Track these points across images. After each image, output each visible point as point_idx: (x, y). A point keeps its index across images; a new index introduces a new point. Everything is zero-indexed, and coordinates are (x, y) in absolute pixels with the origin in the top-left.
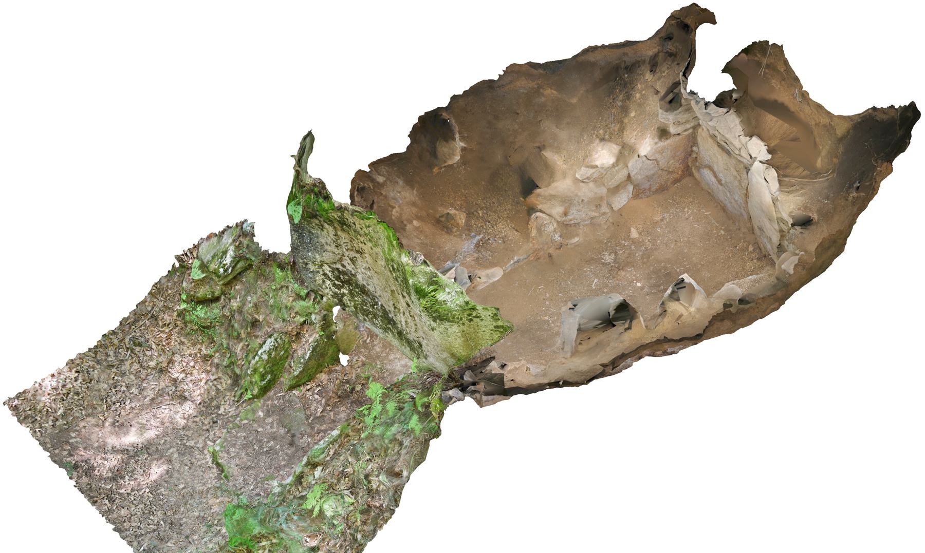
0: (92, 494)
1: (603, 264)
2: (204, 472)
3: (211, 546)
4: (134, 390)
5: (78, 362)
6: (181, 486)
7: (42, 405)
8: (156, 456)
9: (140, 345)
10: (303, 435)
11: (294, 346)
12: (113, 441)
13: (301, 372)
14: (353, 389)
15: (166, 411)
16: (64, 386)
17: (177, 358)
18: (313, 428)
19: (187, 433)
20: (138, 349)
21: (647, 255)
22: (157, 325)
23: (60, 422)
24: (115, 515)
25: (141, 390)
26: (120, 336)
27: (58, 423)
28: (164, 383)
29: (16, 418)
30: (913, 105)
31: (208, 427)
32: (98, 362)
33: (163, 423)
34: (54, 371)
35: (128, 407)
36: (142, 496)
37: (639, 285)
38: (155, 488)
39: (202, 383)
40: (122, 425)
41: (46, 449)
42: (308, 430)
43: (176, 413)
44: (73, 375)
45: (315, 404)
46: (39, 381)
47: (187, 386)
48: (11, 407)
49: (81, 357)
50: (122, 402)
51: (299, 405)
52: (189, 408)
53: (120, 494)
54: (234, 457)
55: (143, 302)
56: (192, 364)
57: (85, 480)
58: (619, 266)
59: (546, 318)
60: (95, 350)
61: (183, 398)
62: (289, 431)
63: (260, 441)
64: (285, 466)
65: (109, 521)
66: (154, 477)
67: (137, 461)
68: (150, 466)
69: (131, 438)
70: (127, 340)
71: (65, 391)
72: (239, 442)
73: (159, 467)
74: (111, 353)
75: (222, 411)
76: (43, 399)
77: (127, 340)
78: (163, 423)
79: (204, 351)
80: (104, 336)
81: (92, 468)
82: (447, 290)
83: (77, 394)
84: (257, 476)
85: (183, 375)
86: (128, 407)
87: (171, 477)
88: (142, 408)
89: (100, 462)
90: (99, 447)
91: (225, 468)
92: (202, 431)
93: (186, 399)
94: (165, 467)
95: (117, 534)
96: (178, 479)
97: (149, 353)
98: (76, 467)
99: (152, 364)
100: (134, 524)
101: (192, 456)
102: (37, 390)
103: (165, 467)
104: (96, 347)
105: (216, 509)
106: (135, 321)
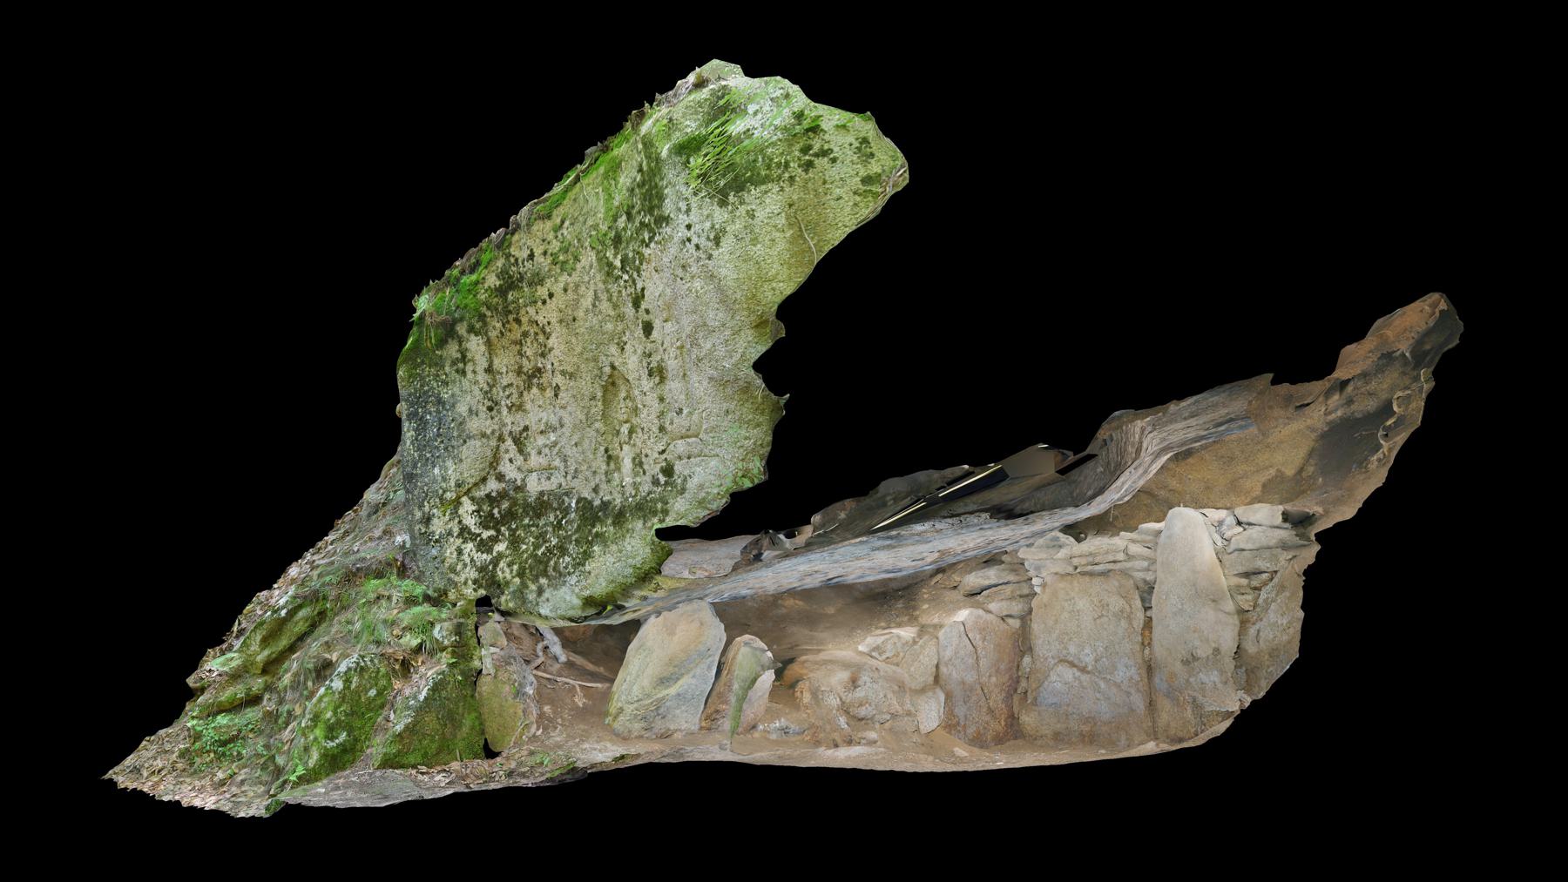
11: (397, 685)
13: (407, 727)
82: (751, 108)
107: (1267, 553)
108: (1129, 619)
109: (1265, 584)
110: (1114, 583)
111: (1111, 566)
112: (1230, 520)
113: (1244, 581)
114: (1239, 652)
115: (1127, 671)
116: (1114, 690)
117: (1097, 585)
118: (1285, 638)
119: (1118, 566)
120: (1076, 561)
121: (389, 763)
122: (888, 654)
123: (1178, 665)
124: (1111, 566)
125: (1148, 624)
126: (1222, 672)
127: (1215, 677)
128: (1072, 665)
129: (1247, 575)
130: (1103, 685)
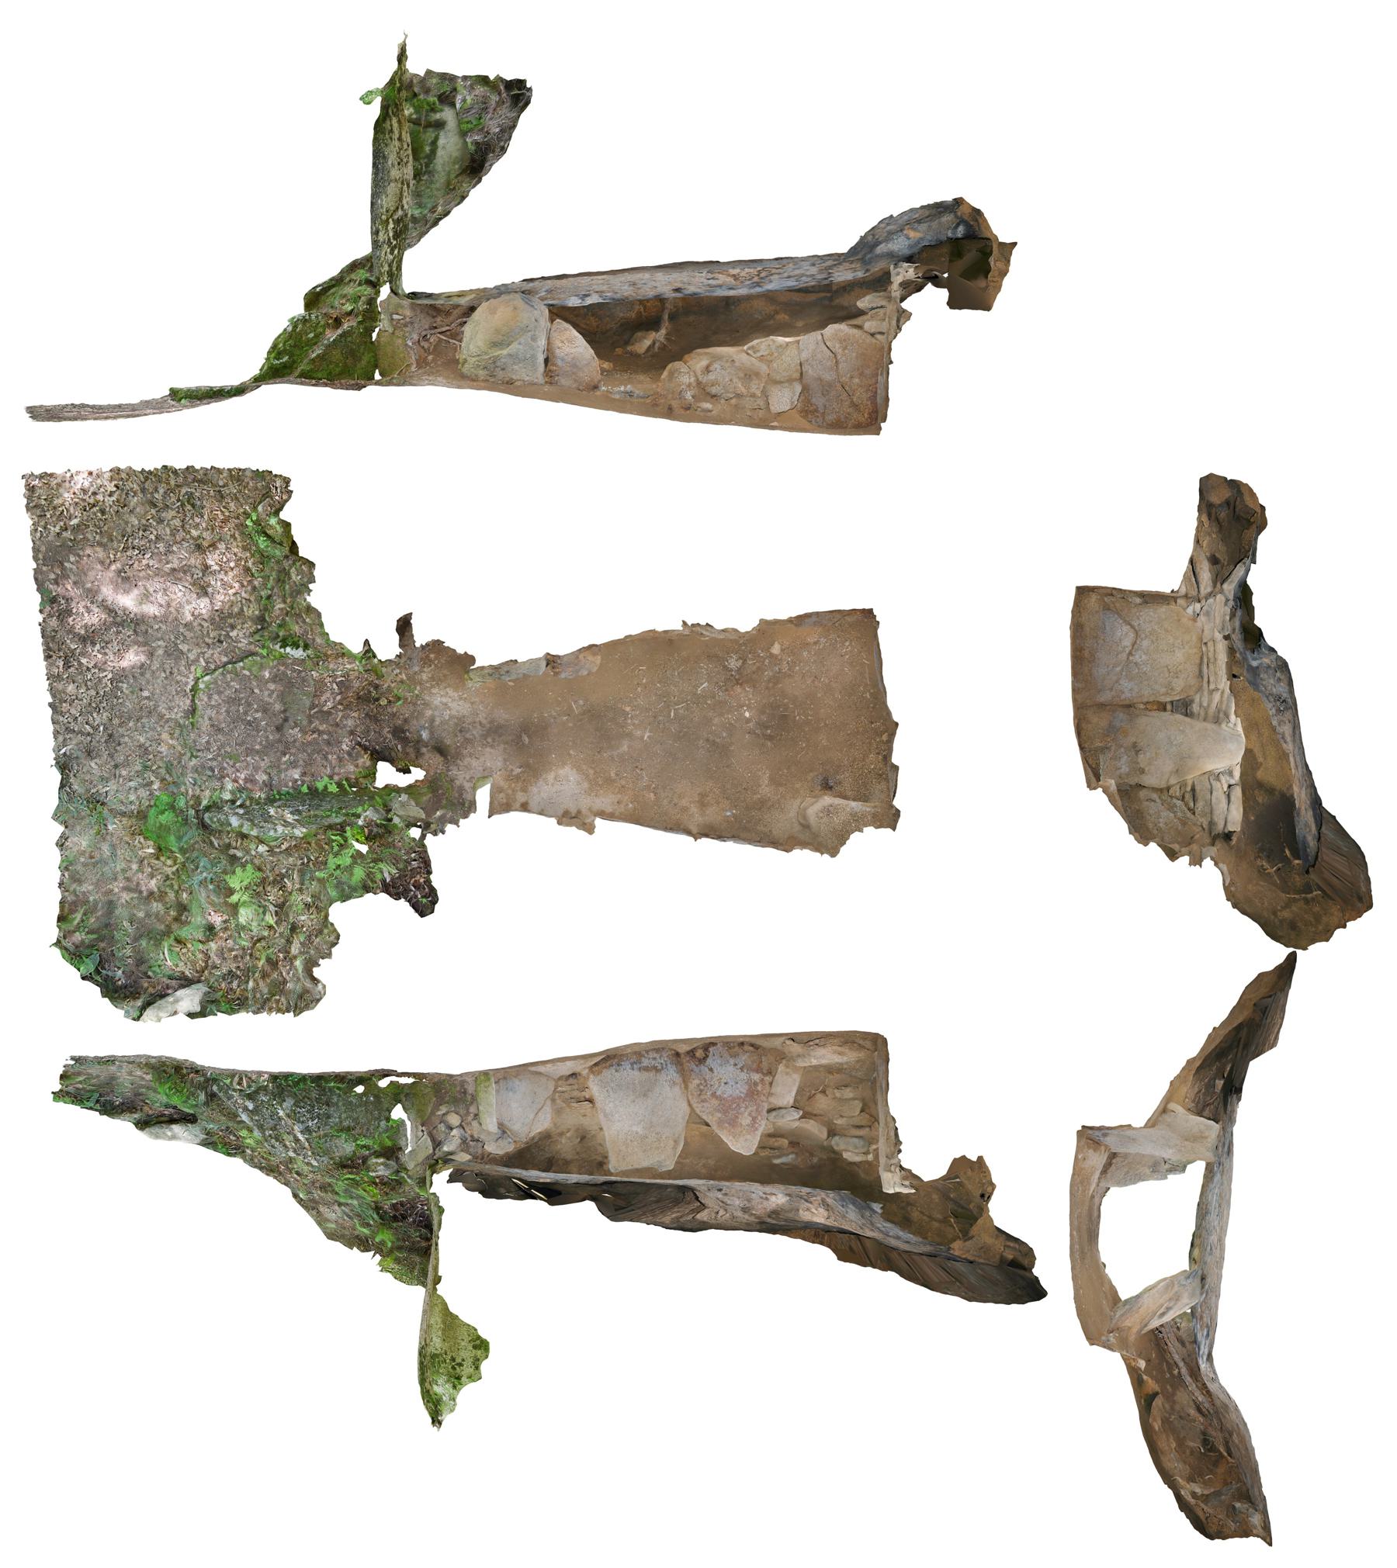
0: (53, 645)
1: (725, 667)
2: (178, 693)
3: (132, 797)
4: (161, 546)
5: (124, 476)
6: (146, 694)
7: (60, 501)
8: (140, 639)
9: (193, 506)
10: (296, 725)
12: (107, 592)
14: (377, 700)
15: (180, 594)
16: (95, 494)
17: (222, 546)
18: (311, 722)
19: (187, 633)
20: (189, 507)
21: (776, 680)
22: (220, 501)
23: (67, 535)
24: (60, 686)
25: (169, 552)
26: (181, 480)
27: (65, 534)
28: (195, 561)
29: (25, 501)
30: (1209, 484)
31: (210, 641)
32: (143, 490)
33: (169, 605)
34: (93, 469)
35: (144, 562)
36: (100, 680)
37: (747, 714)
38: (120, 676)
39: (231, 592)
40: (127, 579)
41: (35, 558)
42: (305, 723)
43: (189, 602)
44: (111, 488)
45: (328, 695)
46: (73, 471)
47: (215, 583)
48: (27, 485)
49: (130, 472)
50: (142, 551)
51: (311, 689)
52: (203, 606)
53: (80, 664)
54: (213, 707)
55: (219, 471)
56: (232, 564)
57: (54, 622)
58: (739, 679)
59: (628, 709)
60: (147, 475)
61: (203, 591)
62: (285, 711)
63: (249, 705)
64: (258, 752)
65: (51, 689)
66: (125, 664)
67: (119, 632)
68: (128, 647)
69: (127, 601)
70: (184, 491)
71: (92, 501)
72: (227, 693)
73: (137, 654)
74: (161, 491)
75: (233, 634)
76: (66, 495)
77: (184, 491)
78: (169, 605)
79: (250, 564)
80: (165, 467)
81: (69, 612)
83: (103, 512)
84: (223, 746)
85: (217, 568)
86: (144, 562)
87: (142, 674)
88: (158, 573)
89: (81, 610)
90: (90, 590)
91: (198, 713)
92: (200, 641)
93: (206, 594)
94: (143, 658)
95: (50, 711)
96: (148, 682)
97: (197, 520)
98: (53, 600)
99: (195, 533)
100: (73, 711)
101: (176, 663)
102: (65, 481)
103: (143, 658)
104: (150, 472)
105: (163, 749)
106: (200, 481)
107: (1207, 810)
108: (1167, 694)
109: (1186, 805)
110: (1193, 681)
112: (1232, 782)
113: (1189, 788)
114: (1140, 786)
115: (1128, 689)
117: (1192, 669)
118: (1151, 826)
119: (1205, 685)
120: (1210, 644)
123: (1133, 739)
125: (1162, 707)
126: (1128, 775)
127: (1125, 769)
129: (1193, 790)
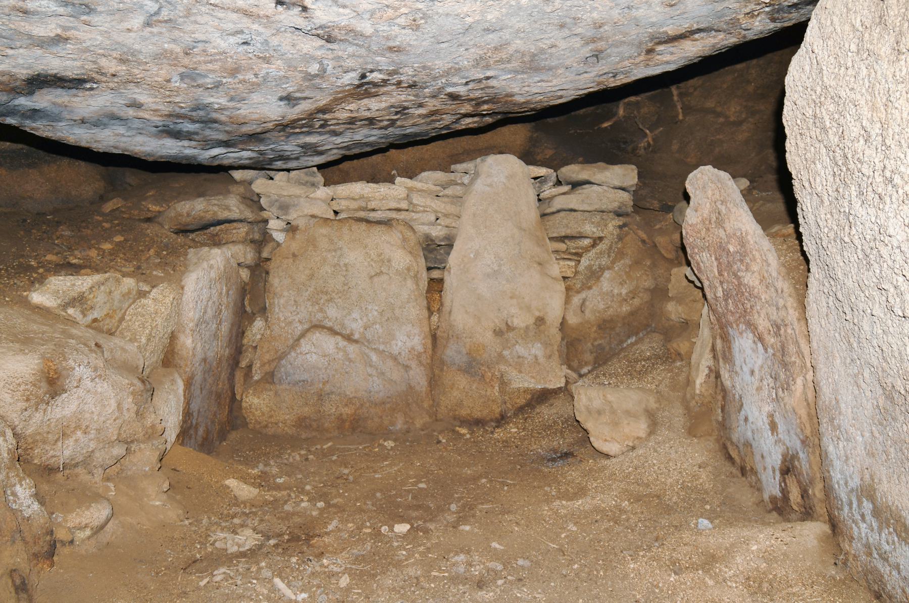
109: (587, 249)
111: (394, 215)
114: (563, 324)
116: (390, 363)
118: (626, 309)
121: (230, 210)
122: (96, 314)
123: (489, 335)
124: (394, 215)
126: (546, 345)
127: (537, 350)
128: (333, 332)
130: (374, 357)
